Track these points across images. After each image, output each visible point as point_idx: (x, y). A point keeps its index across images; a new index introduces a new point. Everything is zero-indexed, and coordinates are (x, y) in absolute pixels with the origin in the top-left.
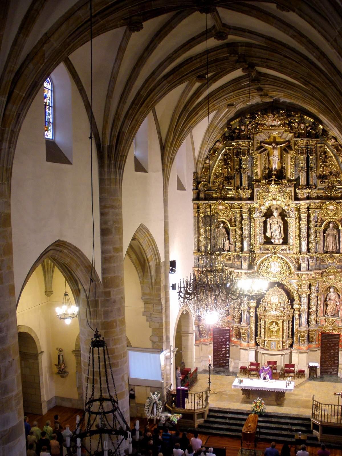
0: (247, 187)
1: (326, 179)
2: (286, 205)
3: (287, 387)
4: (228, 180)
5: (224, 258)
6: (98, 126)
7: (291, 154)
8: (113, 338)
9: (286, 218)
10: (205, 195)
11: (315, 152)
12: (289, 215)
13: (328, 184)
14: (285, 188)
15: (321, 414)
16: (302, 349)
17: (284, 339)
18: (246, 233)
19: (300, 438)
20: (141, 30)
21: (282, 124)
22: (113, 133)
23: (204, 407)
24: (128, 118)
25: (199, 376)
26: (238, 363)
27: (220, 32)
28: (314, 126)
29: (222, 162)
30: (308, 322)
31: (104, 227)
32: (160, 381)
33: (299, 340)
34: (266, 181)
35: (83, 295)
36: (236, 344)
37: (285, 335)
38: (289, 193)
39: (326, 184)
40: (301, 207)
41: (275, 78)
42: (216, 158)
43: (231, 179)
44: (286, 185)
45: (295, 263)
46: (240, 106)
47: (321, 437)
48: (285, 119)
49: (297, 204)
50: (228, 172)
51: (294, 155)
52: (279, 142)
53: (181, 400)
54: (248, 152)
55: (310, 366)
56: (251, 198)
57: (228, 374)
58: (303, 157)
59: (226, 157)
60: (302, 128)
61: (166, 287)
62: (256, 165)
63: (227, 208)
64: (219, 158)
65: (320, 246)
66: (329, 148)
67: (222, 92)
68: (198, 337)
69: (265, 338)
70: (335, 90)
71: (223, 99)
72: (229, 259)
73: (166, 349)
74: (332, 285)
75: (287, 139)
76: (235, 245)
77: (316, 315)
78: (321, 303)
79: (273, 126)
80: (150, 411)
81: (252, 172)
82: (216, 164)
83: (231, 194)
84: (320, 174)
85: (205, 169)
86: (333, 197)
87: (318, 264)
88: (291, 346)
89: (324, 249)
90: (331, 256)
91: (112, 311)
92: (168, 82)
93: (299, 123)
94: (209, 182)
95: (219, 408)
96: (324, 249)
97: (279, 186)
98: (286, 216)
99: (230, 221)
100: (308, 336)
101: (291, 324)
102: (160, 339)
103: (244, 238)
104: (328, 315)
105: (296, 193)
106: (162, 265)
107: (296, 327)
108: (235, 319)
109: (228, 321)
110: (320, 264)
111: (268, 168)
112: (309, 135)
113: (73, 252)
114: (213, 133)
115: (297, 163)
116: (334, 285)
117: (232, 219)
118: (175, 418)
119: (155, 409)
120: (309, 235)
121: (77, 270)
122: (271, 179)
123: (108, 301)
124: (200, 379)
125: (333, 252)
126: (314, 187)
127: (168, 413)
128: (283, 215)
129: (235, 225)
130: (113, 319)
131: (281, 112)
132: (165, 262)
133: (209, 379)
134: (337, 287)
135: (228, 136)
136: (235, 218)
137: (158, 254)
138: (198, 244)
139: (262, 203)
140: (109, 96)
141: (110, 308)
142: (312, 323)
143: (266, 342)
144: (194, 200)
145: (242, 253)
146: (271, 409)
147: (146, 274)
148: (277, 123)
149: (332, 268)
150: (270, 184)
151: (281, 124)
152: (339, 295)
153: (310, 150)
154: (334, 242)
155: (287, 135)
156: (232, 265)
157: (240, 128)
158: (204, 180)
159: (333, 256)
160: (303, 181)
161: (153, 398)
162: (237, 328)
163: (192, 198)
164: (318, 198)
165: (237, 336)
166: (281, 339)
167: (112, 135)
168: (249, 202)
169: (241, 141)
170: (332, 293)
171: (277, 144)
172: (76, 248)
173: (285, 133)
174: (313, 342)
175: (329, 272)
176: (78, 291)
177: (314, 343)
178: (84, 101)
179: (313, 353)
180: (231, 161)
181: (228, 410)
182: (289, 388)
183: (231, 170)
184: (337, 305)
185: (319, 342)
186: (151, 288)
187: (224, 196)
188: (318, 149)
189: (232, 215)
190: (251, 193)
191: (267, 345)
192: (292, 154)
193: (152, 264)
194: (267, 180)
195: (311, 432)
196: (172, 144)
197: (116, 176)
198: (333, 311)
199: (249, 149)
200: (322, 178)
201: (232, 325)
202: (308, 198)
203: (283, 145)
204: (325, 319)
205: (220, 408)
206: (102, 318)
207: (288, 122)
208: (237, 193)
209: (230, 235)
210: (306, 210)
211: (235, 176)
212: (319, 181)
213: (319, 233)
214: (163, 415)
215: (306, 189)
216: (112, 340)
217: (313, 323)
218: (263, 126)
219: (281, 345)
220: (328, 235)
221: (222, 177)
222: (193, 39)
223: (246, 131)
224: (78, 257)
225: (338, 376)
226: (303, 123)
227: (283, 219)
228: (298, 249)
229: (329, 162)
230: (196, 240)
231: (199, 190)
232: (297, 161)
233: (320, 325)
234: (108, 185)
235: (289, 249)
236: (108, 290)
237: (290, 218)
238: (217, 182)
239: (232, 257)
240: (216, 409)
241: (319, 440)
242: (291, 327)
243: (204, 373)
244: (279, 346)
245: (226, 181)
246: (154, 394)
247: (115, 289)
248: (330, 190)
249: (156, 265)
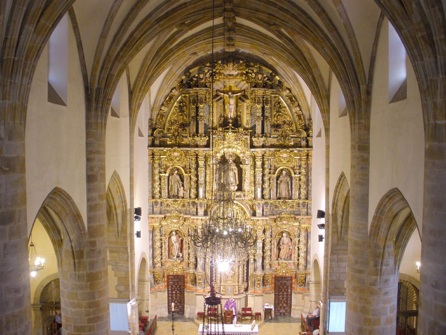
0: (204, 135)
1: (280, 128)
2: (241, 153)
3: (252, 330)
6: (87, 67)
7: (248, 102)
9: (241, 166)
10: (160, 142)
11: (270, 102)
12: (245, 163)
13: (282, 133)
14: (241, 136)
16: (257, 293)
17: (240, 284)
21: (240, 74)
22: (102, 75)
24: (118, 60)
25: (159, 323)
26: (195, 309)
28: (271, 78)
31: (90, 173)
32: (126, 332)
33: (254, 284)
34: (222, 129)
35: (66, 246)
41: (249, 29)
42: (171, 105)
43: (186, 126)
45: (250, 209)
46: (201, 54)
48: (243, 69)
49: (253, 152)
50: (183, 119)
51: (250, 105)
52: (235, 91)
54: (206, 100)
56: (208, 146)
58: (259, 106)
59: (181, 104)
60: (260, 78)
61: (132, 234)
64: (174, 105)
66: (283, 99)
69: (221, 283)
71: (193, 47)
72: (184, 206)
73: (132, 298)
75: (243, 89)
78: (274, 248)
79: (230, 75)
81: (208, 120)
83: (186, 141)
84: (274, 123)
85: (160, 116)
86: (286, 145)
87: (271, 210)
88: (246, 290)
89: (277, 195)
90: (284, 202)
92: (160, 26)
93: (257, 74)
94: (164, 129)
96: (277, 195)
97: (235, 134)
98: (241, 163)
99: (184, 168)
100: (263, 280)
101: (245, 268)
102: (127, 288)
105: (251, 141)
106: (128, 212)
107: (251, 271)
108: (190, 266)
109: (183, 268)
110: (273, 210)
111: (224, 116)
112: (265, 86)
113: (65, 200)
114: (171, 80)
115: (252, 112)
116: (286, 230)
117: (187, 165)
120: (263, 182)
124: (158, 327)
125: (285, 198)
126: (268, 135)
128: (238, 162)
129: (190, 172)
131: (241, 62)
132: (130, 209)
133: (173, 326)
134: (289, 231)
136: (190, 165)
137: (125, 201)
138: (153, 191)
139: (218, 151)
141: (95, 259)
142: (267, 267)
143: (222, 287)
145: (198, 200)
147: (111, 222)
148: (235, 73)
149: (285, 214)
150: (227, 132)
152: (291, 239)
153: (266, 100)
154: (287, 189)
155: (244, 85)
156: (186, 212)
157: (199, 76)
159: (286, 202)
160: (258, 130)
162: (194, 274)
163: (147, 145)
164: (272, 146)
165: (192, 282)
166: (237, 284)
167: (101, 77)
168: (206, 149)
169: (199, 89)
170: (285, 238)
171: (234, 93)
173: (242, 82)
174: (267, 285)
175: (282, 218)
176: (60, 241)
177: (268, 286)
178: (77, 39)
179: (268, 295)
180: (186, 108)
182: (254, 330)
183: (186, 117)
186: (117, 236)
187: (179, 143)
188: (273, 99)
189: (186, 162)
193: (119, 211)
196: (140, 89)
198: (286, 255)
199: (206, 97)
200: (276, 127)
201: (188, 271)
202: (263, 146)
204: (278, 263)
206: (88, 269)
207: (245, 72)
208: (193, 141)
209: (185, 182)
211: (190, 123)
213: (273, 180)
215: (262, 137)
217: (267, 267)
220: (281, 182)
221: (178, 124)
223: (204, 79)
225: (291, 317)
226: (261, 74)
227: (238, 166)
230: (150, 187)
231: (154, 137)
233: (273, 268)
235: (244, 196)
237: (245, 166)
238: (171, 129)
239: (186, 204)
242: (246, 271)
243: (161, 321)
244: (235, 290)
245: (181, 128)
247: (100, 239)
248: (283, 139)
249: (123, 212)
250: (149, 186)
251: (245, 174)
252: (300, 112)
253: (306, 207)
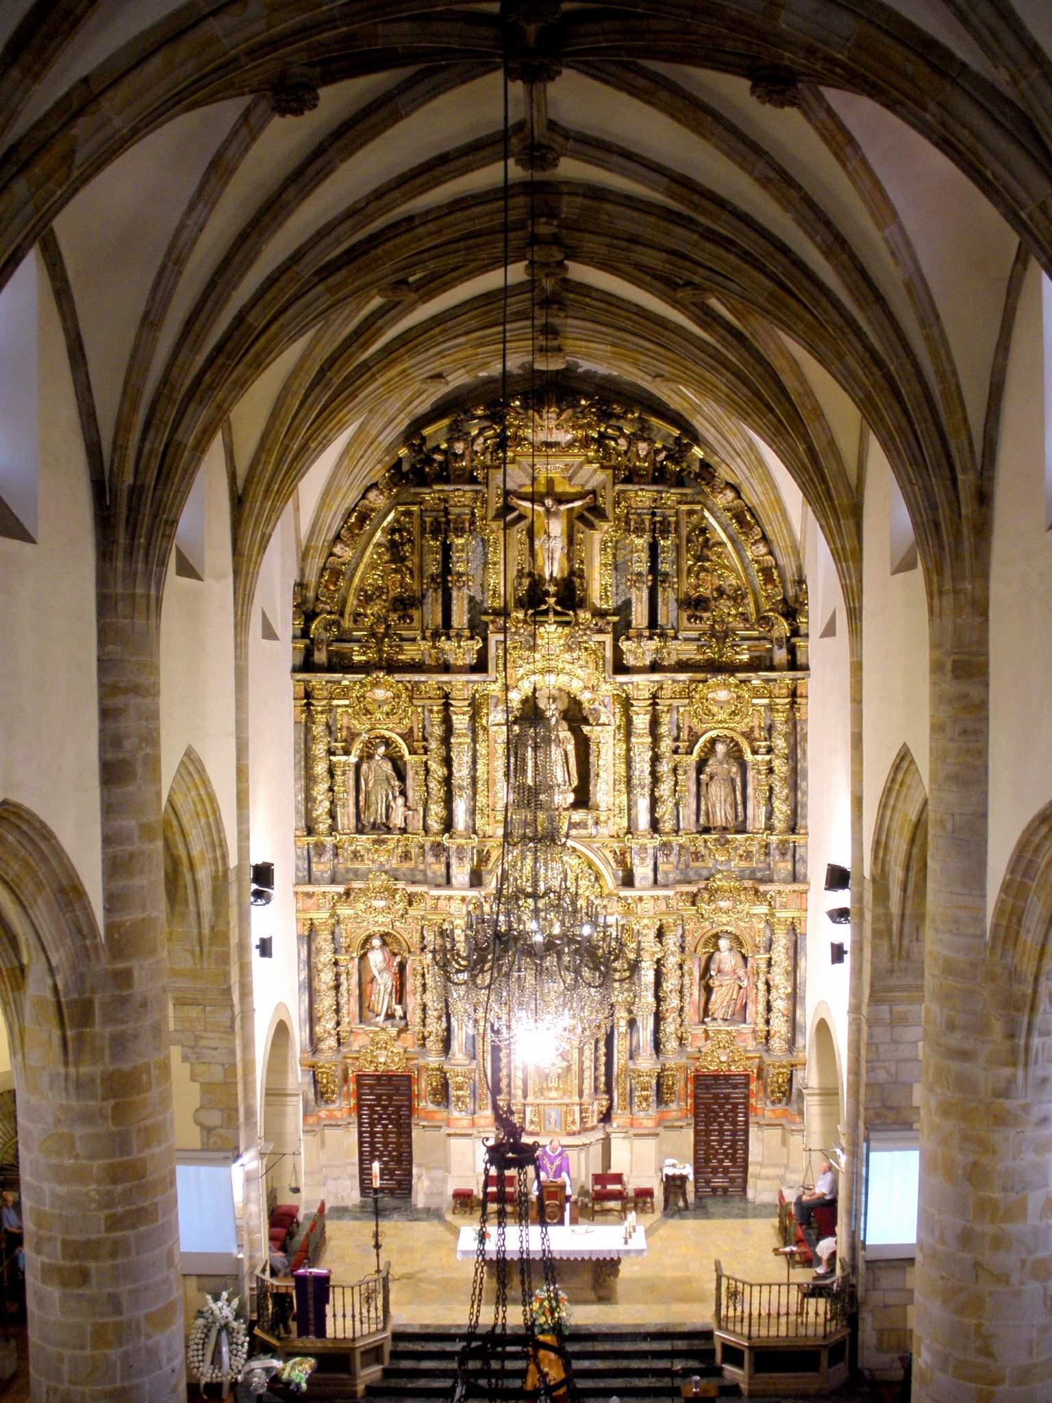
0: (467, 633)
1: (706, 610)
2: (586, 688)
3: (626, 1242)
4: (405, 609)
5: (390, 853)
7: (603, 532)
8: (142, 1124)
9: (586, 729)
10: (331, 655)
13: (713, 626)
15: (750, 1315)
16: (641, 1126)
17: (586, 1099)
18: (461, 773)
19: (696, 1393)
20: (306, 113)
21: (580, 441)
22: (148, 446)
23: (380, 1326)
24: (197, 397)
27: (540, 146)
28: (678, 452)
29: (382, 553)
30: (657, 1046)
31: (110, 756)
32: (230, 1254)
33: (631, 1098)
34: (526, 615)
36: (433, 1119)
37: (588, 1085)
38: (595, 652)
39: (705, 626)
40: (635, 694)
42: (364, 538)
43: (412, 605)
44: (589, 628)
45: (614, 865)
47: (749, 1384)
48: (590, 426)
49: (622, 684)
51: (612, 537)
52: (563, 494)
53: (311, 1309)
54: (472, 523)
55: (667, 1176)
56: (480, 666)
57: (414, 1215)
58: (641, 541)
59: (397, 537)
60: (642, 453)
61: (243, 947)
62: (495, 564)
63: (399, 697)
64: (375, 540)
65: (686, 811)
66: (716, 518)
67: (440, 333)
68: (312, 1103)
69: (525, 1097)
70: (859, 347)
72: (406, 856)
73: (247, 1149)
74: (726, 928)
75: (588, 487)
79: (549, 445)
80: (209, 1358)
81: (482, 585)
82: (366, 559)
83: (410, 653)
84: (687, 594)
85: (330, 576)
86: (726, 663)
87: (682, 866)
88: (606, 1117)
90: (723, 841)
91: (136, 1036)
93: (632, 439)
94: (342, 614)
95: (422, 1326)
97: (567, 630)
98: (586, 721)
99: (407, 736)
101: (603, 1050)
103: (456, 791)
104: (714, 1019)
105: (618, 652)
106: (232, 876)
107: (619, 1059)
108: (429, 1044)
110: (687, 866)
111: (530, 575)
112: (659, 477)
114: (362, 461)
115: (620, 560)
117: (415, 730)
118: (299, 1372)
119: (225, 1349)
120: (655, 779)
121: (36, 901)
122: (544, 607)
123: (123, 1001)
125: (725, 829)
126: (671, 632)
127: (272, 1357)
130: (142, 1061)
131: (583, 402)
132: (239, 868)
133: (376, 1235)
135: (407, 472)
137: (222, 844)
138: (308, 812)
140: (150, 321)
142: (669, 1047)
143: (528, 1110)
144: (295, 670)
146: (581, 1315)
149: (727, 878)
150: (542, 623)
151: (575, 440)
152: (745, 958)
153: (661, 523)
155: (594, 476)
156: (414, 876)
157: (450, 446)
158: (328, 608)
159: (727, 841)
160: (639, 616)
161: (217, 1312)
162: (440, 1069)
163: (289, 666)
164: (682, 666)
165: (435, 1095)
166: (576, 1099)
169: (452, 488)
171: (560, 499)
172: (44, 826)
173: (586, 467)
174: (672, 1101)
175: (716, 890)
176: (18, 973)
177: (673, 1106)
178: (66, 331)
179: (673, 1134)
180: (413, 548)
181: (453, 1331)
183: (412, 577)
184: (740, 987)
185: (689, 1101)
186: (198, 953)
187: (389, 660)
188: (684, 519)
189: (414, 718)
190: (478, 652)
191: (536, 1119)
192: (607, 532)
193: (203, 874)
194: (530, 612)
195: (719, 1372)
197: (149, 589)
199: (473, 514)
200: (694, 605)
201: (421, 1062)
202: (655, 667)
203: (578, 504)
204: (706, 1031)
205: (428, 1326)
206: (107, 1059)
207: (596, 435)
208: (433, 651)
209: (409, 782)
210: (787, 700)
211: (423, 596)
212: (685, 615)
213: (685, 772)
214: (258, 1365)
215: (650, 638)
216: (139, 1131)
217: (671, 1045)
219: (577, 1117)
220: (712, 778)
221: (385, 601)
222: (443, 159)
223: (468, 458)
224: (45, 859)
225: (746, 1199)
226: (644, 440)
227: (576, 731)
229: (714, 558)
230: (301, 797)
231: (312, 640)
232: (621, 553)
233: (689, 1049)
235: (597, 823)
236: (120, 965)
237: (599, 728)
238: (366, 616)
239: (414, 851)
240: (417, 1330)
241: (746, 1393)
242: (603, 1059)
243: (339, 1218)
244: (570, 1119)
245: (395, 611)
246: (216, 1298)
249: (215, 878)
250: (296, 796)
252: (769, 558)
253: (789, 857)
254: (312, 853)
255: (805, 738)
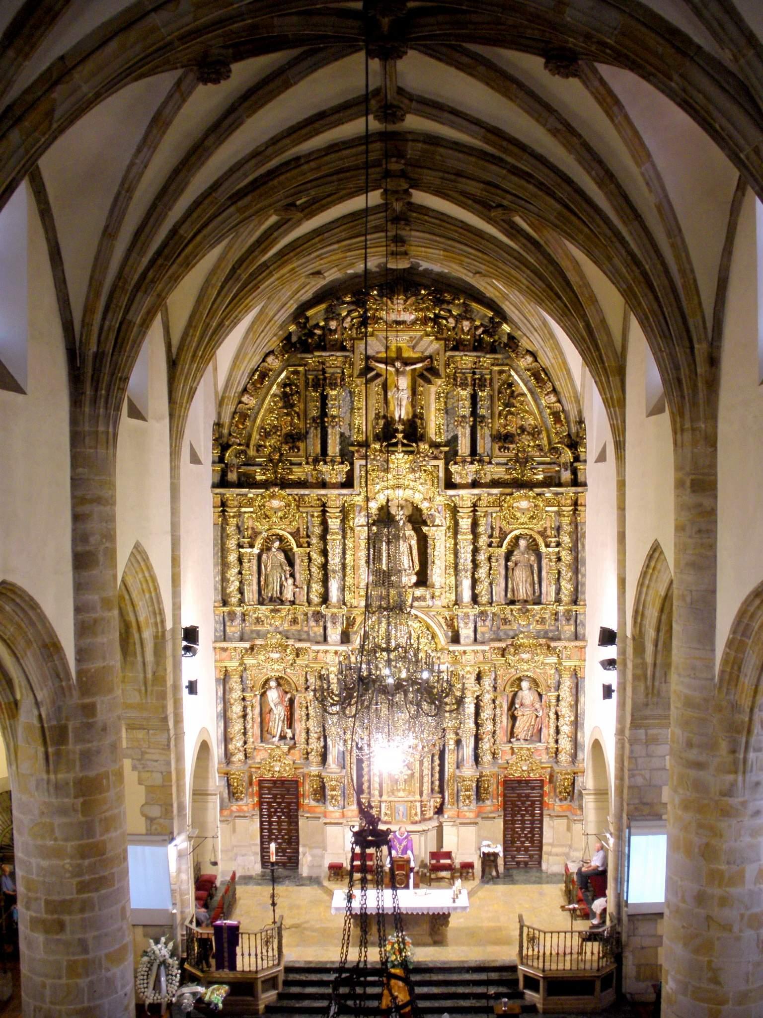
0: (339, 459)
1: (512, 443)
2: (425, 499)
3: (454, 901)
4: (294, 442)
5: (283, 619)
7: (438, 386)
8: (103, 816)
9: (425, 529)
10: (240, 475)
13: (517, 454)
15: (544, 954)
16: (465, 817)
17: (425, 797)
18: (334, 561)
19: (505, 1011)
20: (222, 82)
21: (421, 320)
22: (107, 323)
23: (276, 962)
24: (143, 288)
28: (492, 328)
29: (277, 401)
30: (477, 759)
31: (80, 549)
32: (167, 910)
33: (458, 797)
34: (381, 446)
36: (314, 812)
37: (426, 787)
38: (431, 473)
39: (512, 454)
40: (460, 503)
42: (264, 390)
43: (299, 439)
44: (427, 455)
45: (445, 627)
46: (332, 275)
47: (544, 1004)
48: (428, 309)
49: (451, 496)
51: (444, 390)
52: (409, 358)
53: (226, 950)
54: (343, 380)
55: (484, 853)
56: (348, 483)
57: (300, 881)
58: (465, 393)
59: (288, 389)
60: (466, 329)
61: (176, 687)
62: (359, 409)
63: (289, 506)
64: (272, 392)
65: (498, 588)
66: (519, 376)
67: (319, 242)
69: (381, 796)
70: (623, 252)
72: (295, 621)
73: (179, 834)
74: (526, 673)
75: (427, 354)
76: (309, 587)
77: (492, 740)
79: (398, 323)
80: (151, 985)
81: (350, 425)
82: (265, 406)
83: (298, 473)
84: (498, 431)
85: (239, 418)
86: (526, 481)
87: (494, 628)
88: (440, 811)
90: (524, 610)
91: (98, 752)
93: (459, 319)
95: (306, 962)
97: (411, 457)
98: (425, 523)
99: (295, 534)
101: (437, 762)
103: (331, 574)
104: (518, 740)
105: (448, 473)
106: (168, 636)
107: (449, 768)
108: (311, 757)
110: (499, 628)
111: (385, 417)
112: (478, 346)
114: (263, 334)
115: (449, 406)
117: (301, 530)
118: (217, 995)
119: (163, 979)
120: (475, 565)
121: (26, 654)
122: (394, 440)
125: (526, 601)
126: (487, 459)
127: (198, 985)
130: (103, 770)
131: (423, 292)
132: (173, 630)
133: (273, 896)
135: (295, 343)
137: (161, 612)
138: (224, 589)
140: (109, 233)
142: (485, 759)
143: (383, 805)
144: (214, 486)
146: (422, 954)
148: (409, 317)
149: (527, 637)
150: (393, 452)
151: (417, 319)
152: (540, 695)
153: (480, 379)
155: (431, 345)
156: (300, 635)
157: (327, 324)
158: (238, 441)
159: (528, 611)
160: (464, 447)
161: (157, 952)
163: (210, 483)
164: (495, 484)
165: (315, 794)
166: (418, 797)
169: (328, 354)
171: (406, 362)
172: (32, 599)
173: (425, 339)
174: (488, 799)
175: (520, 646)
176: (13, 706)
177: (488, 802)
178: (48, 240)
179: (488, 823)
180: (299, 398)
181: (328, 966)
184: (537, 716)
185: (500, 799)
186: (143, 691)
187: (282, 479)
188: (496, 376)
189: (300, 521)
190: (347, 473)
191: (388, 812)
192: (440, 386)
193: (148, 634)
194: (385, 444)
195: (521, 996)
197: (108, 428)
199: (343, 373)
200: (504, 439)
201: (305, 770)
202: (475, 484)
203: (419, 365)
204: (512, 748)
205: (310, 962)
206: (78, 768)
207: (432, 316)
208: (314, 472)
209: (297, 567)
210: (571, 508)
211: (307, 433)
212: (497, 446)
213: (497, 560)
214: (187, 990)
215: (472, 463)
216: (101, 820)
217: (487, 758)
218: (376, 323)
219: (419, 810)
220: (516, 564)
221: (279, 436)
222: (321, 116)
223: (339, 332)
224: (32, 624)
225: (541, 870)
226: (467, 319)
227: (418, 531)
228: (454, 598)
229: (518, 405)
230: (218, 578)
231: (226, 465)
232: (450, 401)
233: (500, 761)
234: (90, 448)
235: (433, 597)
236: (87, 701)
237: (434, 528)
238: (265, 447)
239: (301, 618)
240: (302, 965)
241: (541, 1011)
242: (437, 769)
243: (246, 884)
244: (413, 812)
245: (286, 443)
246: (157, 942)
249: (156, 637)
250: (215, 578)
251: (434, 548)
252: (558, 405)
253: (572, 622)
254: (227, 619)
255: (584, 536)
